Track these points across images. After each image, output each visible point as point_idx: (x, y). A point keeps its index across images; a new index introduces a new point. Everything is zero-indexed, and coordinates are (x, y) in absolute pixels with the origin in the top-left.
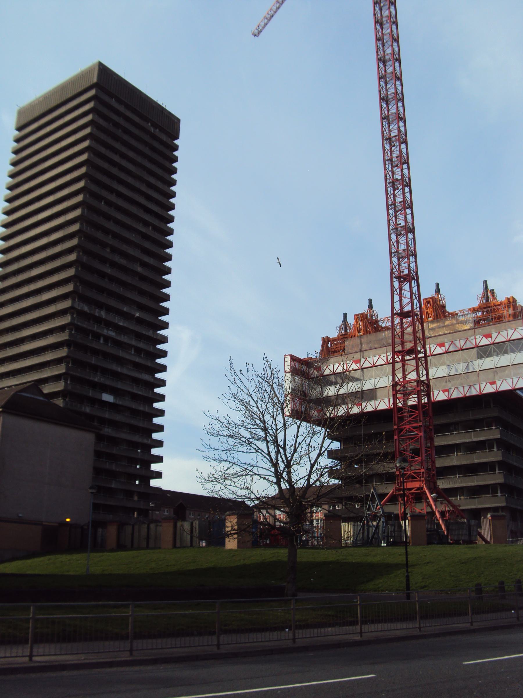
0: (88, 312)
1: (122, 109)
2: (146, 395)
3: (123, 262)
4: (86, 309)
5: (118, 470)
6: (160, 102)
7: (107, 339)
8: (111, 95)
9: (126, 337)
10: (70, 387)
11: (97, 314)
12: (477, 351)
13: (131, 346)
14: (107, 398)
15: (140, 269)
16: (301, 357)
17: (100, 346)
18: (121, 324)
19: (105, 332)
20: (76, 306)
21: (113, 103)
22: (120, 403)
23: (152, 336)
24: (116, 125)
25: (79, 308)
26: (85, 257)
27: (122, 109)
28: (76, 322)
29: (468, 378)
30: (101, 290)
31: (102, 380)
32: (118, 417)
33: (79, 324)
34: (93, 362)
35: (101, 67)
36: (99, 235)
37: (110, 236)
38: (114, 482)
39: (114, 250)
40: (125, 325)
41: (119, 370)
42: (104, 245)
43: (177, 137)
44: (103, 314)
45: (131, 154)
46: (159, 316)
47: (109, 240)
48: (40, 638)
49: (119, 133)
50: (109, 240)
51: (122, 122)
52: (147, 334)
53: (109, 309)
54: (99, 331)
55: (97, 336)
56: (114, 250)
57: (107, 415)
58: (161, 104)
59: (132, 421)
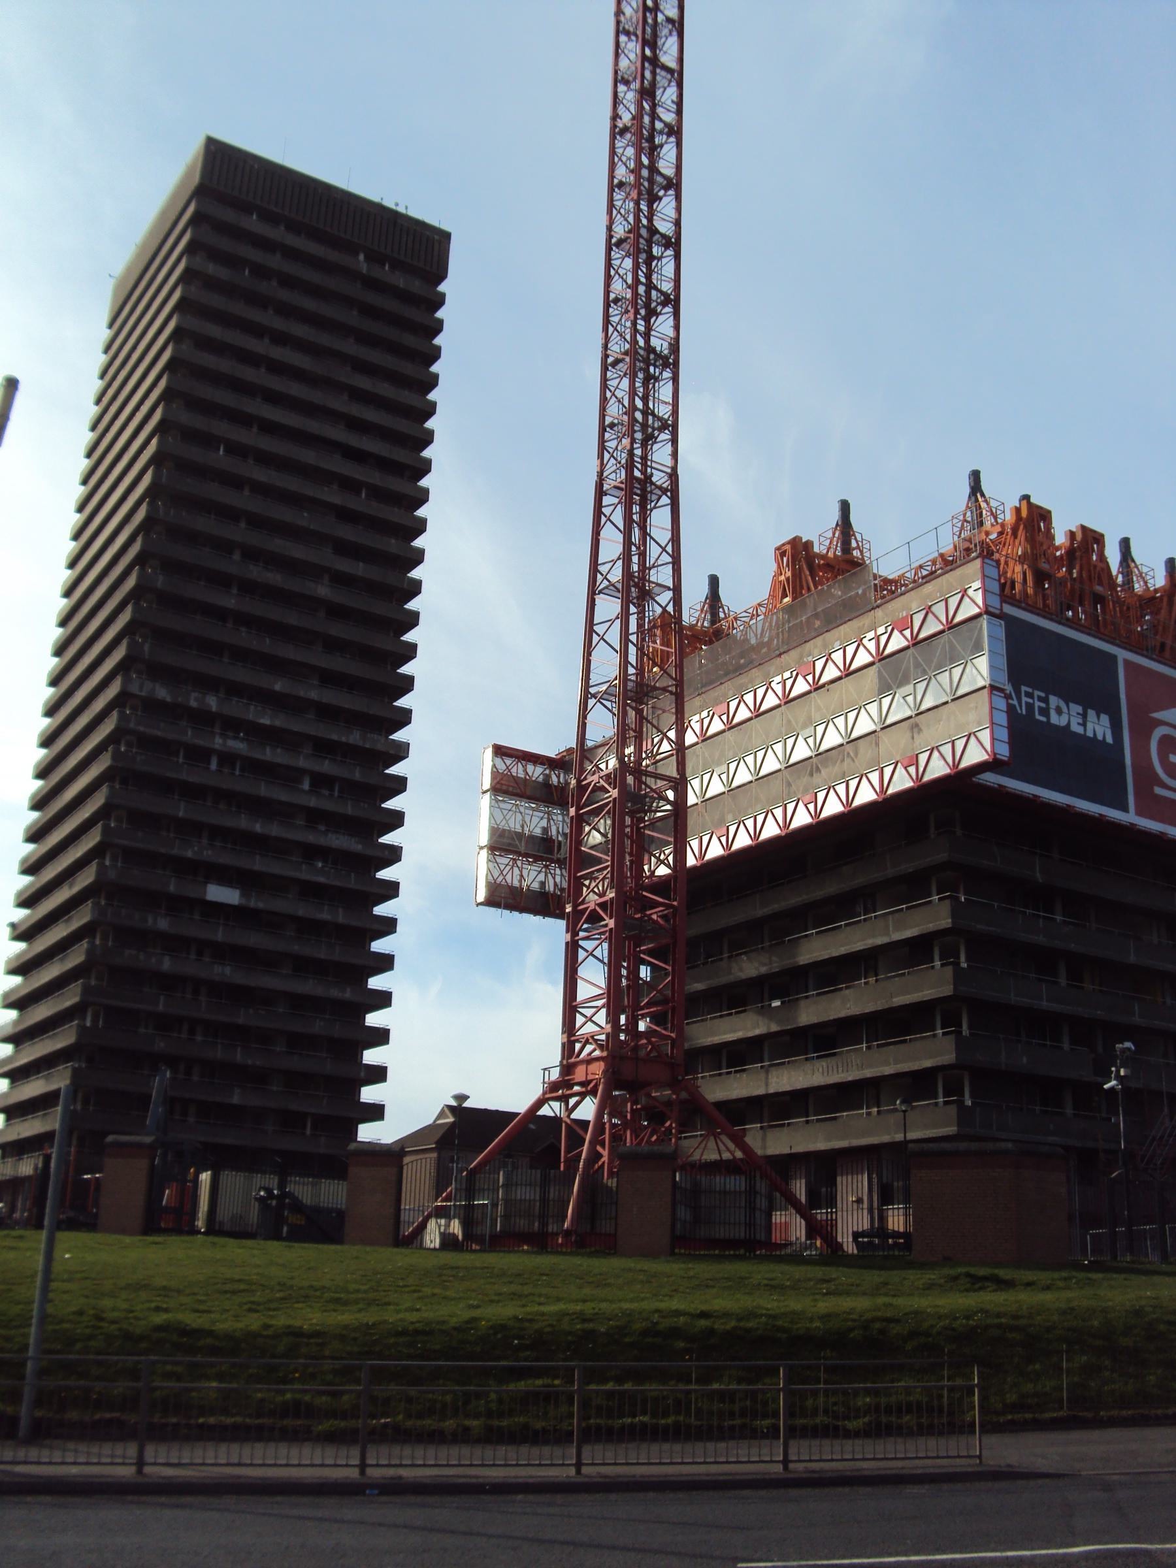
0: (169, 699)
1: (277, 233)
2: (338, 884)
3: (275, 578)
4: (162, 693)
5: (250, 1062)
6: (389, 203)
7: (227, 759)
8: (245, 208)
9: (279, 750)
10: (112, 875)
11: (193, 704)
12: (879, 671)
13: (303, 772)
14: (218, 893)
15: (323, 590)
16: (552, 754)
17: (211, 774)
18: (266, 721)
19: (218, 742)
20: (134, 689)
21: (252, 223)
22: (261, 905)
23: (360, 743)
24: (260, 272)
25: (143, 694)
26: (161, 578)
27: (277, 233)
28: (132, 725)
29: (856, 754)
30: (212, 648)
31: (208, 854)
32: (254, 939)
33: (142, 729)
34: (181, 814)
35: (212, 147)
36: (204, 524)
37: (243, 525)
38: (237, 1091)
39: (252, 554)
40: (278, 723)
41: (258, 828)
42: (224, 547)
43: (442, 276)
44: (213, 703)
45: (299, 330)
46: (396, 700)
47: (239, 533)
48: (592, 1435)
49: (268, 288)
50: (239, 533)
51: (275, 261)
52: (344, 739)
53: (235, 690)
54: (200, 742)
55: (199, 755)
56: (252, 554)
57: (220, 935)
58: (393, 207)
59: (296, 947)
